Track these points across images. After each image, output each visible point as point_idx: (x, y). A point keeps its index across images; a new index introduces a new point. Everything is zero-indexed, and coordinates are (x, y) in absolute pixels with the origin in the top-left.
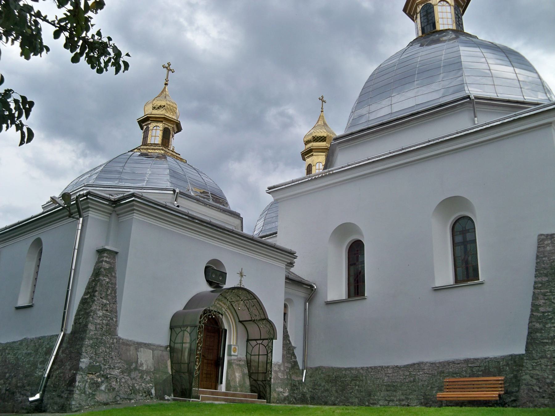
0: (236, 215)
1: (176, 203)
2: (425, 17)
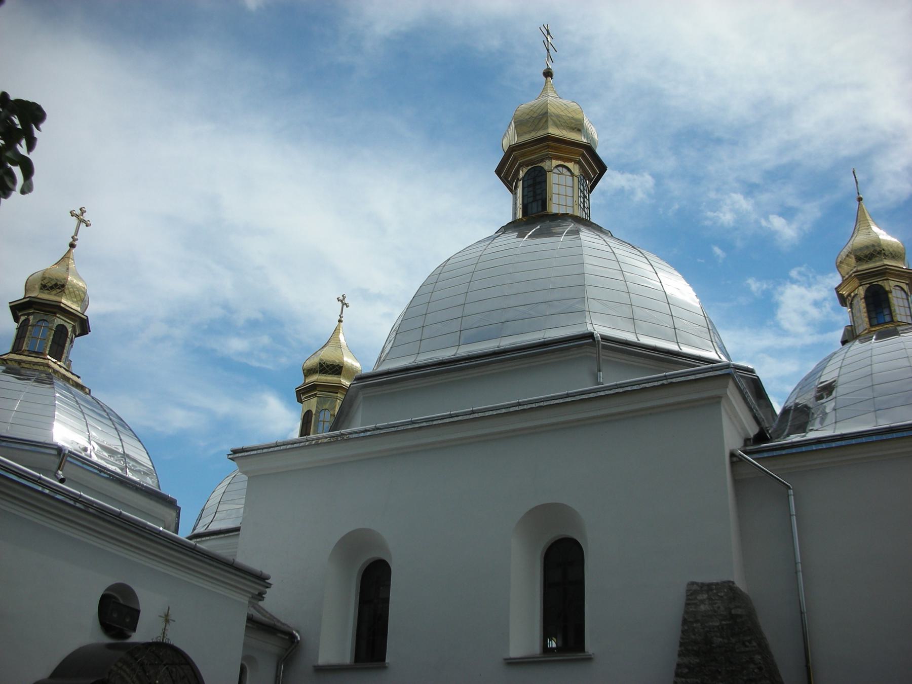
0: (170, 503)
1: (60, 472)
2: (531, 189)
